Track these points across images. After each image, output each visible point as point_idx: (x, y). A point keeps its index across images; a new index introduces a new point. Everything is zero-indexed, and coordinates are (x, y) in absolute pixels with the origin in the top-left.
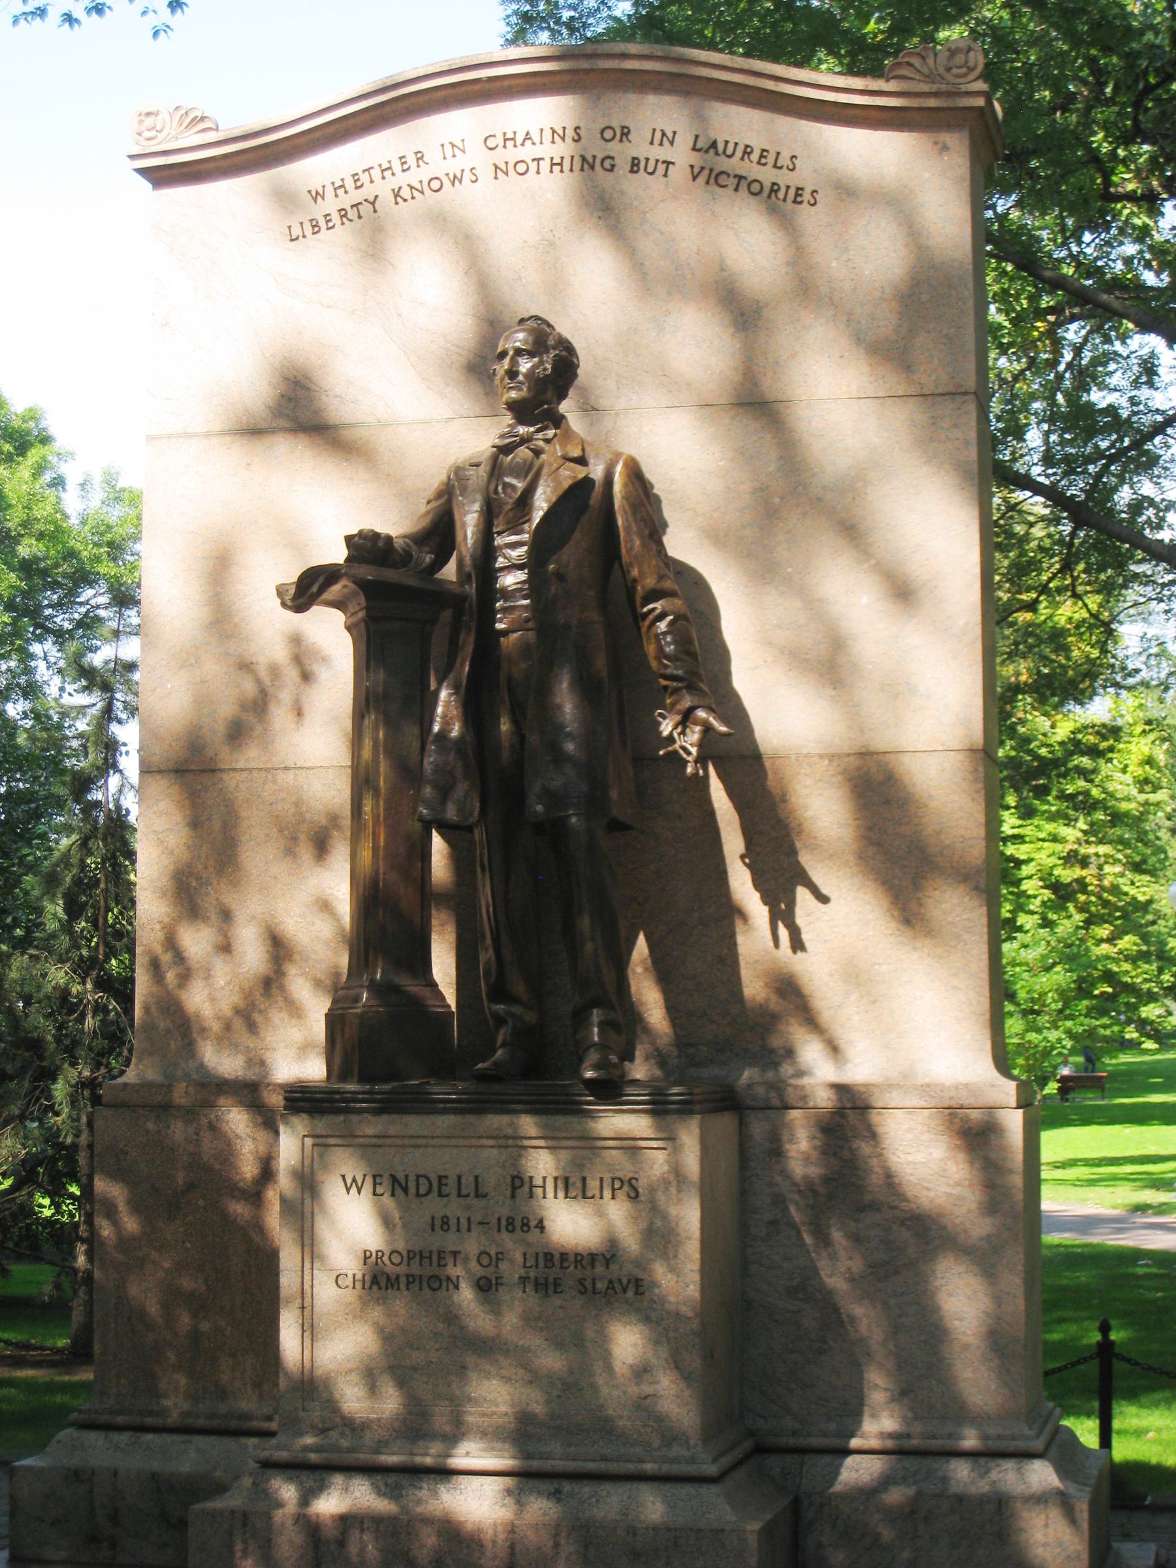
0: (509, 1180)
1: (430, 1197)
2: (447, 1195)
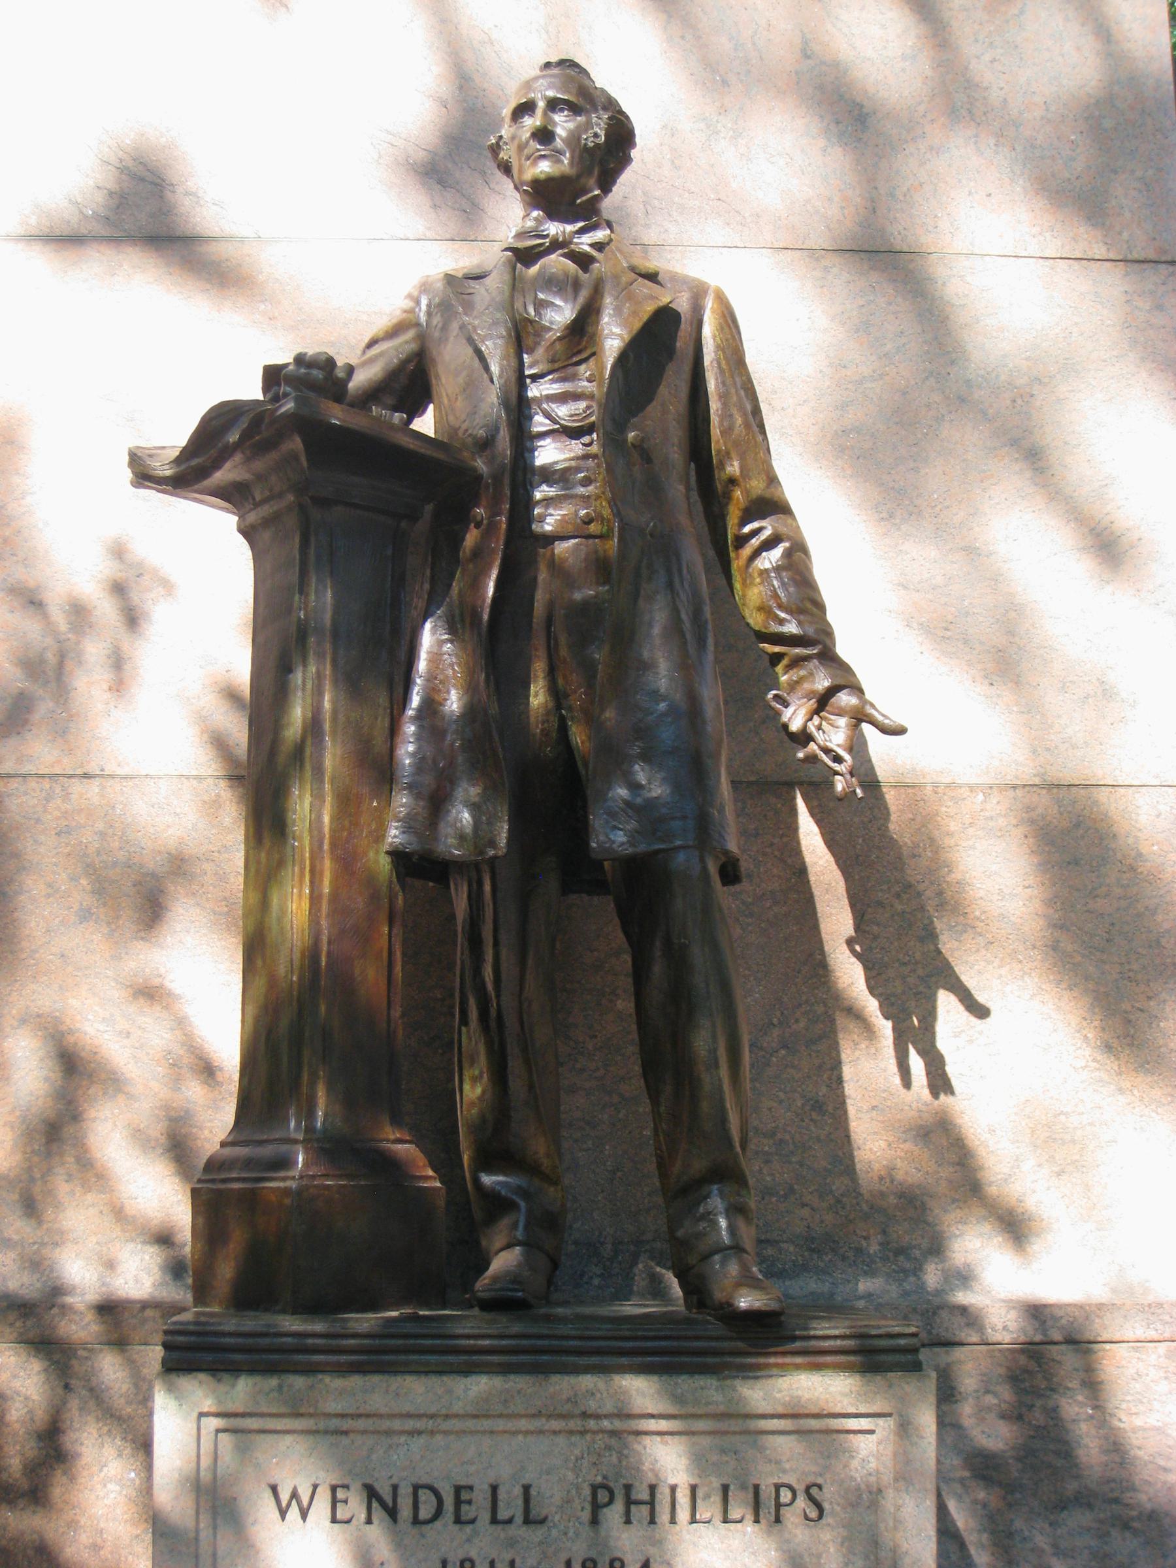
0: (587, 1491)
1: (438, 1524)
2: (473, 1521)
